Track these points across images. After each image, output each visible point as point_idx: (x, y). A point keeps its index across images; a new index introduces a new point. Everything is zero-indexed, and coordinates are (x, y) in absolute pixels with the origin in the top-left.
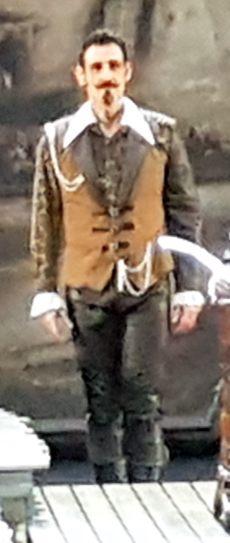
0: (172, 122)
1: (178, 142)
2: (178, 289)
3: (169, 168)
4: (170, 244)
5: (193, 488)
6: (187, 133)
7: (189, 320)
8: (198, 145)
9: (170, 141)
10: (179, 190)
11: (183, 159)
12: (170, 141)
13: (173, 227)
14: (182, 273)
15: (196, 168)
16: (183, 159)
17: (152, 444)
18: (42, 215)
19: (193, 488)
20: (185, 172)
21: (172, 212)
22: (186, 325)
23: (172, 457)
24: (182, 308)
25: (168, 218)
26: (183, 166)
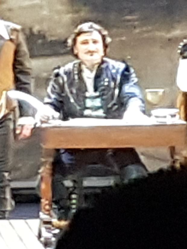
0: (19, 27)
1: (22, 38)
2: (21, 116)
3: (17, 53)
4: (17, 95)
5: (27, 223)
6: (28, 32)
7: (27, 132)
8: (32, 37)
9: (17, 37)
10: (21, 64)
11: (24, 48)
12: (17, 37)
13: (20, 85)
14: (23, 109)
15: (30, 50)
16: (24, 48)
17: (67, 96)
18: (47, 169)
19: (27, 223)
20: (25, 54)
21: (19, 75)
22: (25, 135)
23: (16, 203)
24: (22, 126)
25: (17, 80)
26: (24, 51)
